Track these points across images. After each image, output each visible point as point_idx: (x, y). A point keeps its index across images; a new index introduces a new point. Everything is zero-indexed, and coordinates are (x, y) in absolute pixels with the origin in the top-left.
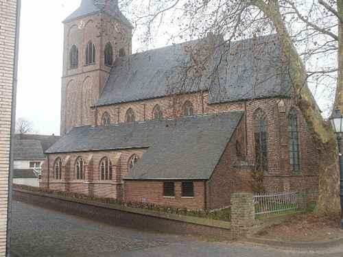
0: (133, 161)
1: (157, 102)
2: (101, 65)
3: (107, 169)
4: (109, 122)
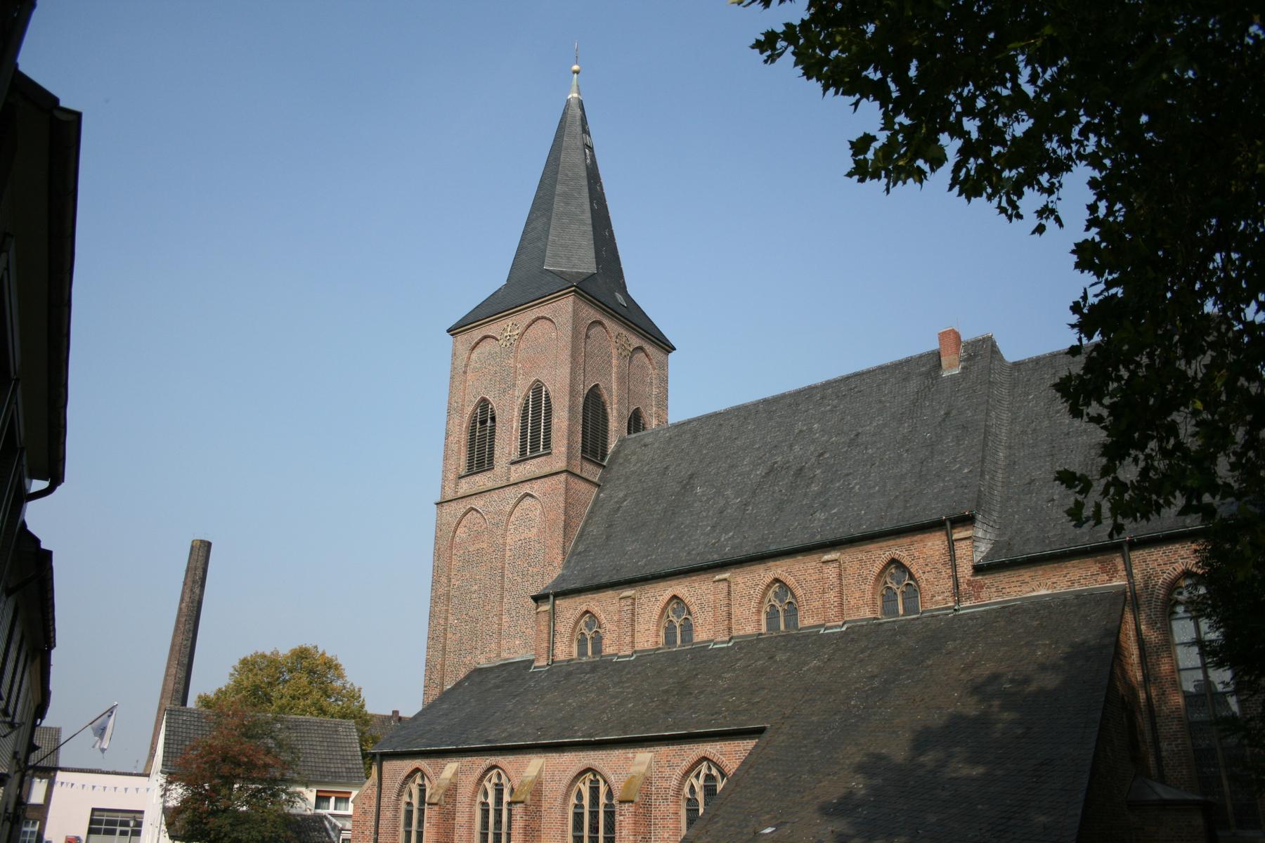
0: (699, 784)
1: (779, 569)
2: (570, 457)
3: (594, 815)
4: (597, 649)
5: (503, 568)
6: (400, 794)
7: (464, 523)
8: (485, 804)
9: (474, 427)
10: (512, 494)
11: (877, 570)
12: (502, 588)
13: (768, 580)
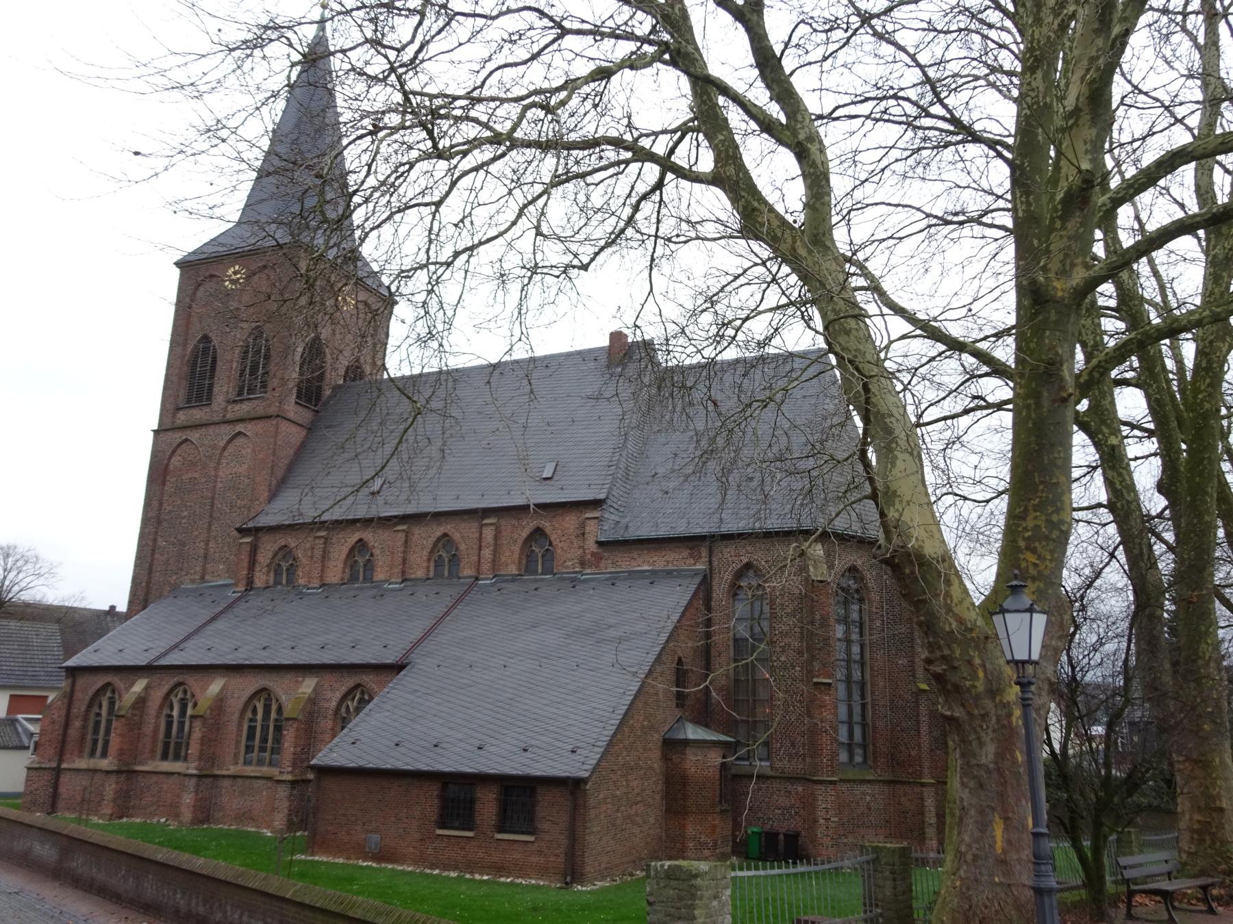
3: (265, 728)
5: (213, 498)
6: (90, 706)
7: (179, 452)
8: (170, 716)
9: (196, 357)
10: (226, 431)
11: (525, 535)
12: (211, 516)
13: (439, 534)
